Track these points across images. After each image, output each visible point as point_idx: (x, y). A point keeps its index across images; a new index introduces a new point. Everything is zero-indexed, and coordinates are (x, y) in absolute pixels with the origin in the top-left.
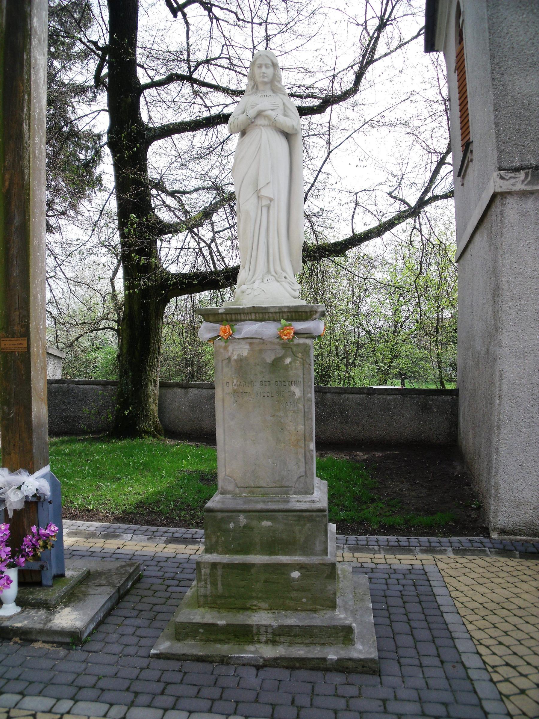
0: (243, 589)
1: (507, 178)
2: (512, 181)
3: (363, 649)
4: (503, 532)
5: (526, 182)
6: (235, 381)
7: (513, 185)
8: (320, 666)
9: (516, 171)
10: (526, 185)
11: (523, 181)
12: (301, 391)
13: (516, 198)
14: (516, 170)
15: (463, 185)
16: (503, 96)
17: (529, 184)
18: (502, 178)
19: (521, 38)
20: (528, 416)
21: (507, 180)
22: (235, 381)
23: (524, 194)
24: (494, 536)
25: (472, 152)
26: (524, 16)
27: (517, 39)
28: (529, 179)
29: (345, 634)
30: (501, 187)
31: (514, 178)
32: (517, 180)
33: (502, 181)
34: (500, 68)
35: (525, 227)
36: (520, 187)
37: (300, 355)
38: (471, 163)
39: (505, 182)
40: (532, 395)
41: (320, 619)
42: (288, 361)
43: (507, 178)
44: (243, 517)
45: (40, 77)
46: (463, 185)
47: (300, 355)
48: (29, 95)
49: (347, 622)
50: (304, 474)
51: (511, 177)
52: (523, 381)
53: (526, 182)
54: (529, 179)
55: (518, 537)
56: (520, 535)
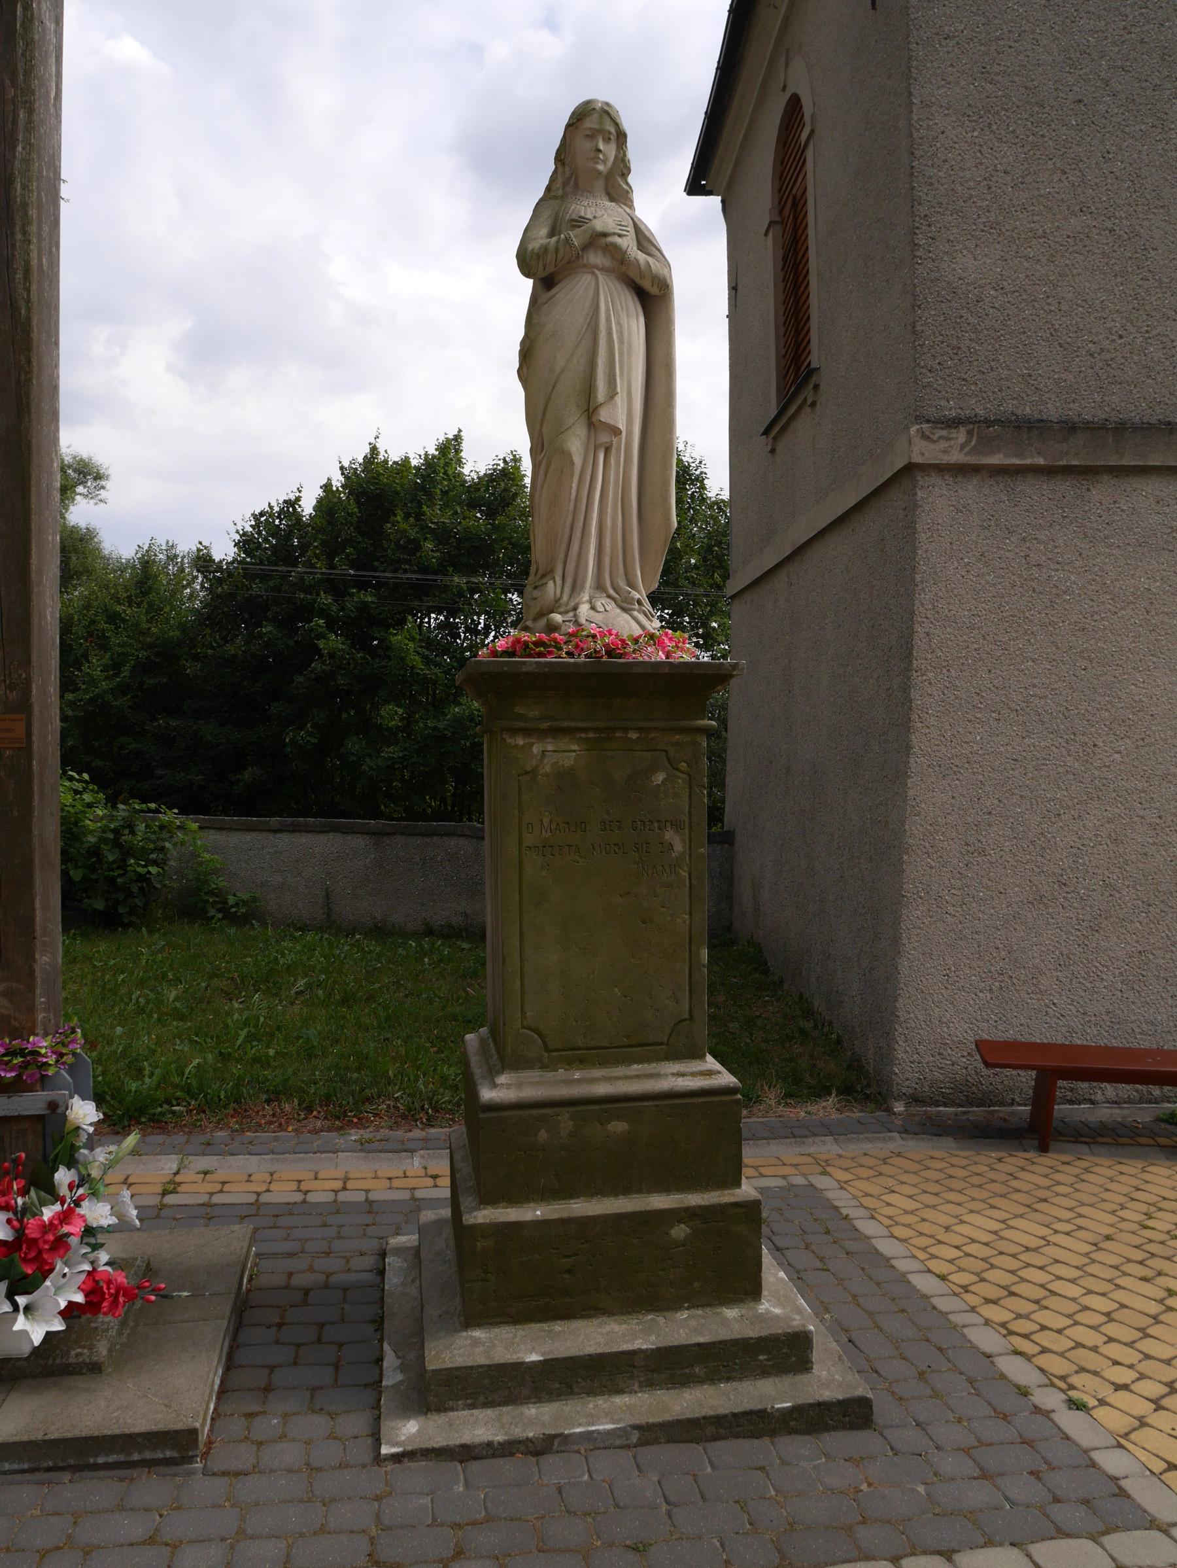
0: (566, 1276)
1: (935, 437)
2: (944, 444)
3: (829, 1378)
4: (915, 1099)
5: (967, 449)
6: (546, 821)
7: (944, 452)
8: (756, 1424)
9: (950, 427)
10: (967, 454)
11: (962, 447)
12: (683, 840)
13: (946, 477)
14: (953, 423)
15: (773, 451)
16: (932, 281)
17: (974, 451)
18: (925, 437)
19: (968, 175)
20: (958, 883)
21: (935, 442)
22: (546, 821)
23: (960, 471)
24: (899, 1107)
25: (816, 387)
26: (976, 134)
27: (962, 174)
28: (973, 443)
29: (788, 1352)
30: (923, 454)
31: (948, 439)
32: (952, 443)
33: (925, 443)
34: (929, 225)
35: (962, 533)
36: (956, 457)
37: (683, 766)
38: (807, 410)
39: (933, 446)
40: (967, 844)
41: (731, 1321)
42: (659, 777)
43: (935, 437)
44: (567, 1115)
45: (50, 75)
46: (773, 451)
47: (683, 766)
48: (30, 111)
49: (797, 1322)
50: (687, 1016)
51: (941, 437)
52: (950, 819)
53: (967, 449)
54: (973, 443)
55: (941, 1108)
56: (945, 1105)
